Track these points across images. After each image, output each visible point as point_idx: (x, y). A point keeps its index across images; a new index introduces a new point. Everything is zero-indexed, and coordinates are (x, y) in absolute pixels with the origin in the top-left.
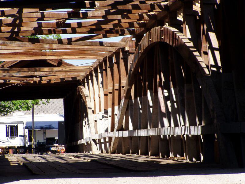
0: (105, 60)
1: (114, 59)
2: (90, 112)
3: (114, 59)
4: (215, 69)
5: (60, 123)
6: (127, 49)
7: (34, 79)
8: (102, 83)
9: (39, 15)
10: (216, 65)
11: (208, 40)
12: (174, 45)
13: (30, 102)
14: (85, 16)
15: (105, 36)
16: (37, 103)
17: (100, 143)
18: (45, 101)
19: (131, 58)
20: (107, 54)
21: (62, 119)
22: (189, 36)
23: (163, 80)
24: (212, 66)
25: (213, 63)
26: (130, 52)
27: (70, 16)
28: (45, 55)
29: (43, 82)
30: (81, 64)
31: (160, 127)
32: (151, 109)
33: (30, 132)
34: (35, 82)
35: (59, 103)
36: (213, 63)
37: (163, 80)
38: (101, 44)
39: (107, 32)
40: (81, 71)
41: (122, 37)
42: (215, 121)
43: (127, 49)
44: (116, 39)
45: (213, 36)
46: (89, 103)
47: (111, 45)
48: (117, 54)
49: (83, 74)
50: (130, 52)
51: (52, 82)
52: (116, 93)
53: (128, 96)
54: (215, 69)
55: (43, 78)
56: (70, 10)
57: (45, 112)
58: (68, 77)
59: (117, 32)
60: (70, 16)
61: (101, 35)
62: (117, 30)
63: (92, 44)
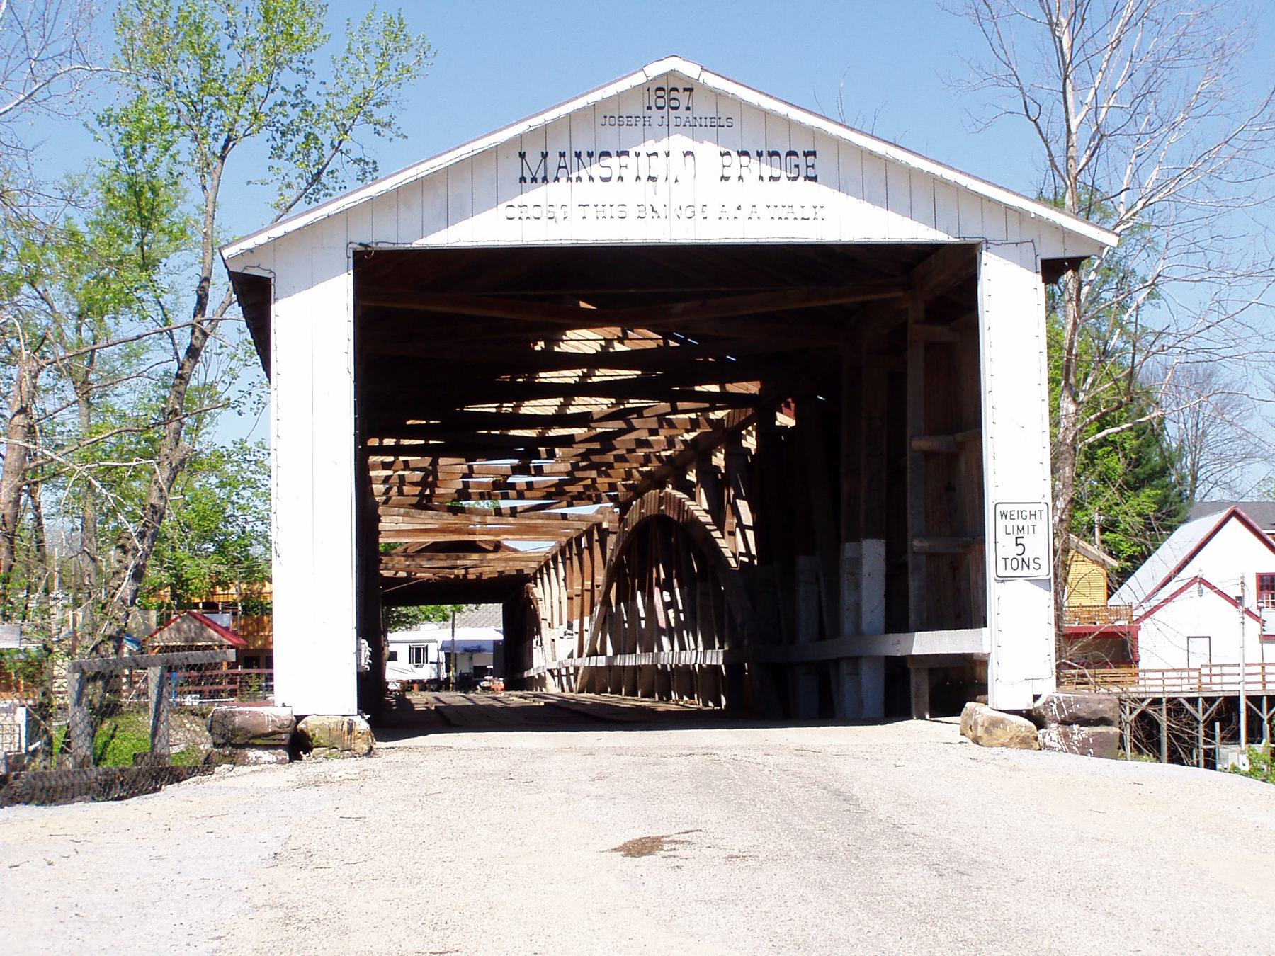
0: (569, 543)
2: (544, 625)
4: (746, 560)
5: (496, 643)
6: (605, 525)
7: (456, 572)
8: (565, 580)
13: (448, 608)
14: (539, 471)
15: (570, 505)
17: (560, 675)
18: (473, 606)
21: (500, 637)
22: (705, 506)
23: (663, 576)
24: (741, 554)
25: (743, 550)
27: (516, 470)
28: (473, 533)
29: (471, 577)
30: (531, 548)
33: (447, 655)
34: (457, 576)
36: (743, 550)
37: (663, 576)
38: (564, 517)
40: (532, 559)
42: (746, 642)
43: (605, 525)
44: (588, 510)
45: (743, 506)
46: (544, 612)
47: (581, 518)
48: (589, 533)
49: (534, 565)
51: (485, 577)
52: (587, 596)
53: (606, 602)
54: (746, 560)
55: (471, 570)
56: (516, 461)
57: (473, 624)
58: (510, 568)
59: (590, 498)
60: (516, 470)
61: (565, 503)
63: (549, 517)
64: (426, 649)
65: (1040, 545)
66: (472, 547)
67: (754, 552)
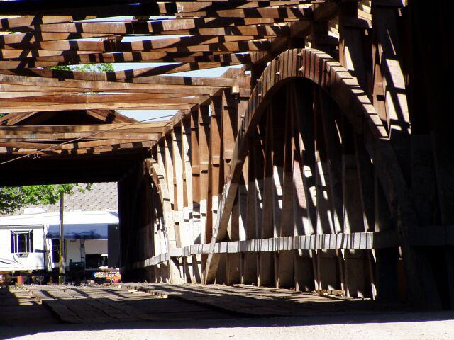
0: (194, 112)
1: (211, 108)
2: (166, 207)
3: (211, 108)
4: (398, 128)
5: (111, 227)
6: (235, 90)
7: (64, 146)
8: (189, 154)
9: (72, 27)
10: (400, 121)
11: (386, 73)
12: (323, 82)
13: (56, 188)
14: (158, 29)
15: (194, 67)
16: (68, 191)
17: (185, 264)
18: (83, 186)
19: (243, 107)
20: (199, 101)
21: (115, 220)
23: (302, 148)
24: (393, 122)
25: (395, 117)
26: (241, 96)
28: (83, 101)
30: (150, 118)
31: (296, 234)
32: (280, 202)
34: (65, 151)
35: (108, 191)
36: (395, 117)
37: (302, 148)
38: (188, 81)
39: (199, 59)
41: (226, 68)
42: (399, 223)
43: (235, 90)
44: (215, 73)
45: (394, 66)
46: (166, 191)
47: (207, 82)
48: (216, 99)
49: (154, 137)
50: (241, 96)
51: (97, 152)
52: (216, 171)
54: (398, 128)
55: (81, 145)
56: (130, 18)
57: (84, 206)
58: (127, 142)
59: (217, 59)
61: (188, 65)
62: (217, 56)
63: (170, 81)
64: (31, 235)
65: (60, 134)
66: (82, 118)
67: (407, 119)
